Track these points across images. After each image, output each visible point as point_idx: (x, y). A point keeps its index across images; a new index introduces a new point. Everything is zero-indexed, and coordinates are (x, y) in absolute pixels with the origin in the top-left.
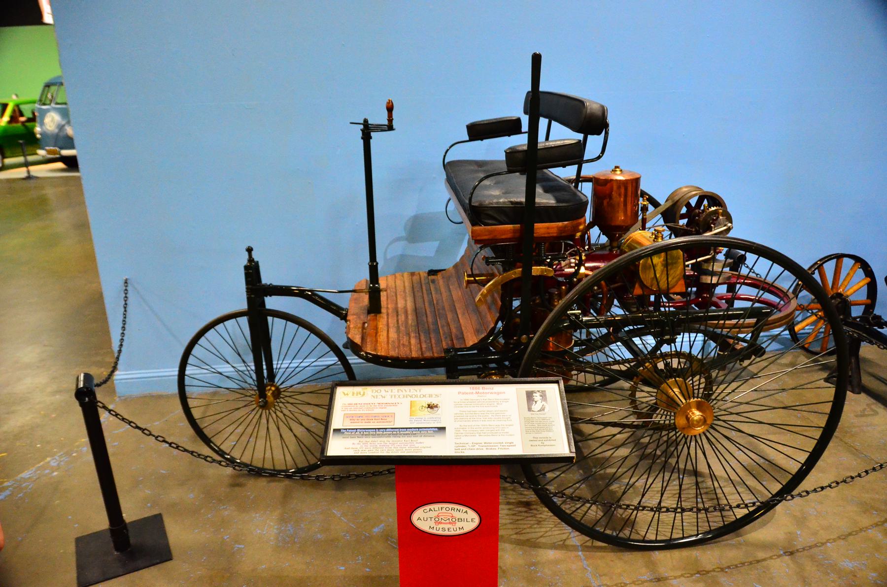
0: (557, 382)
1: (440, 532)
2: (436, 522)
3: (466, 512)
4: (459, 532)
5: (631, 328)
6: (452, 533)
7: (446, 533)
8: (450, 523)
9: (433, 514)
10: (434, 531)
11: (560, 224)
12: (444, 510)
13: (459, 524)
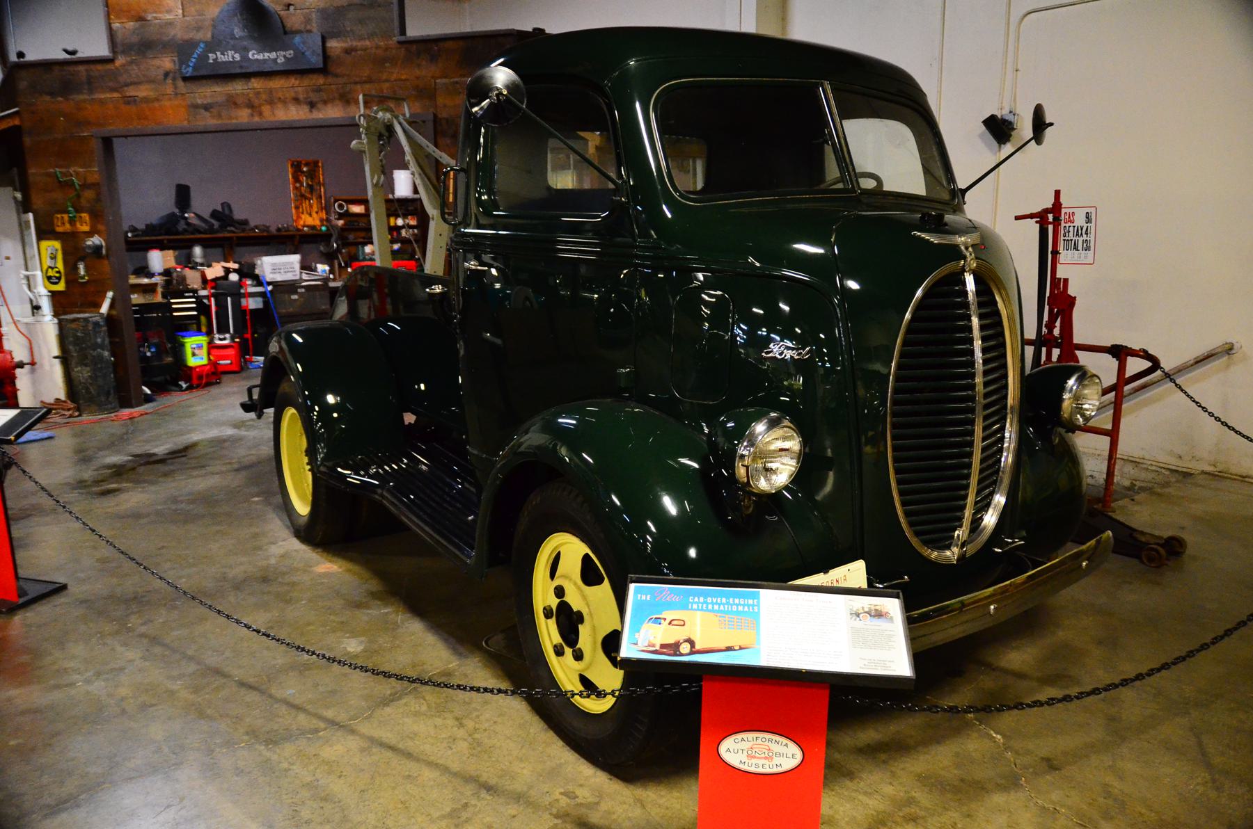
0: (898, 597)
1: (753, 769)
2: (750, 757)
3: (786, 745)
4: (775, 770)
5: (462, 352)
6: (768, 770)
7: (760, 770)
8: (766, 758)
9: (745, 745)
10: (745, 767)
11: (367, 168)
12: (759, 741)
13: (776, 760)
